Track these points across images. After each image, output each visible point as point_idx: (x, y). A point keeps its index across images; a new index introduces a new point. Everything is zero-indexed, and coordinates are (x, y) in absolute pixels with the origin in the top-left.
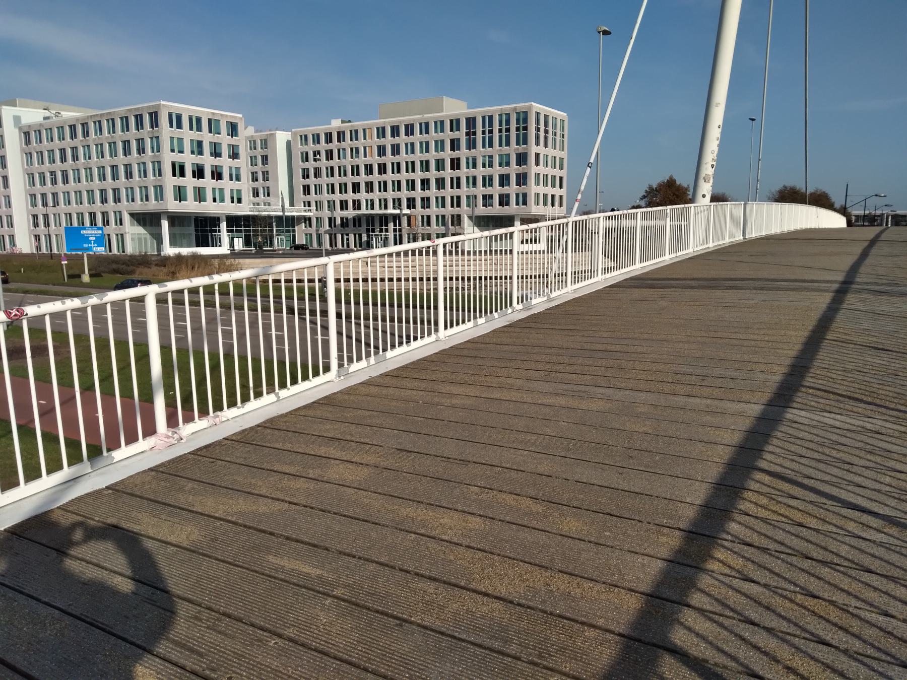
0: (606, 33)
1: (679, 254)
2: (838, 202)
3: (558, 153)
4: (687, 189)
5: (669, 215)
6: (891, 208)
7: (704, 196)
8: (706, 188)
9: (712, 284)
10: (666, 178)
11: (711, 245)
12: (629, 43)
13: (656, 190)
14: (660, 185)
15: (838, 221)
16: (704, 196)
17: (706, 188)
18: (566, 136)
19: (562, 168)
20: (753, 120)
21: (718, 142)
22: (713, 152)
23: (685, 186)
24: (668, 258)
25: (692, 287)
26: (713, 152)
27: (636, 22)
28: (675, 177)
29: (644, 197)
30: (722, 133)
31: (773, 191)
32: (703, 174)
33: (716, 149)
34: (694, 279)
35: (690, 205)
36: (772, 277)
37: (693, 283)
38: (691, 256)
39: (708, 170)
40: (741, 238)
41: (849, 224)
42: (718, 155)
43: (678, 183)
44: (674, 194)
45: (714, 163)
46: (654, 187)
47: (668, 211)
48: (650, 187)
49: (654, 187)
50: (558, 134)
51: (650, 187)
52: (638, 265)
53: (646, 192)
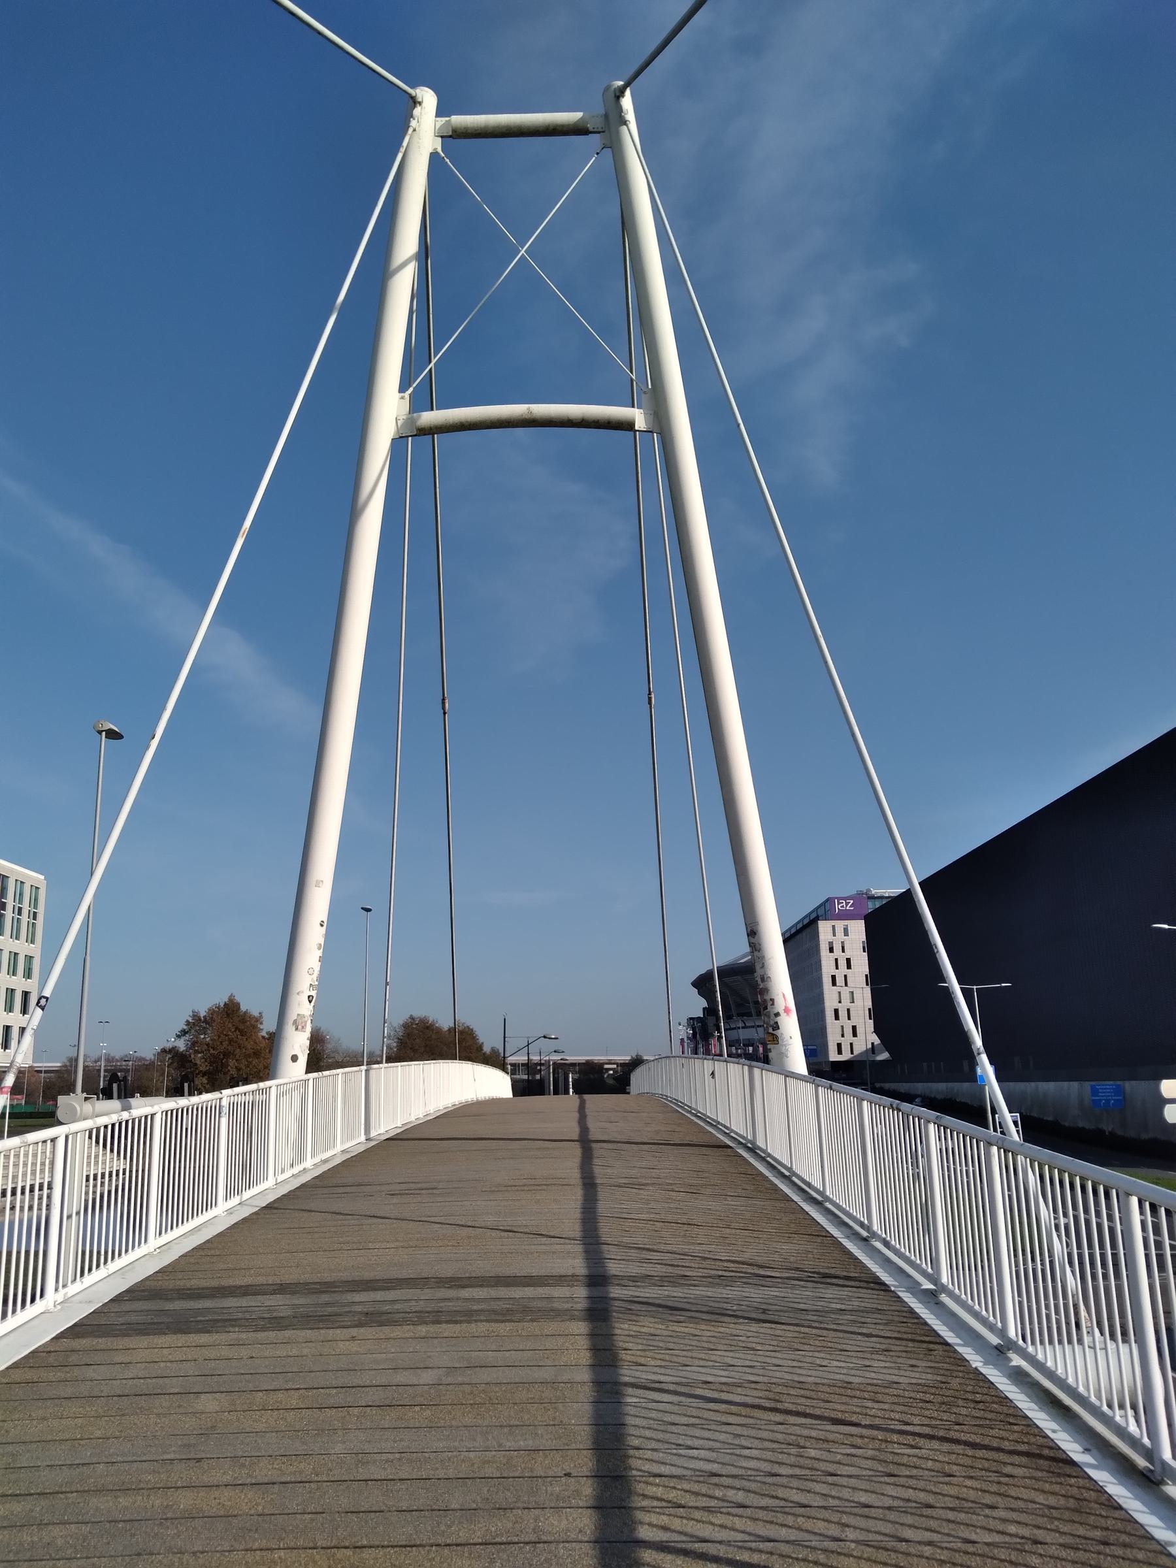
0: (112, 735)
1: (247, 1195)
2: (489, 1040)
3: (22, 947)
4: (258, 1020)
5: (225, 1110)
6: (553, 1045)
7: (294, 1058)
8: (297, 1043)
9: (324, 1304)
10: (221, 999)
11: (309, 1163)
12: (148, 747)
13: (205, 1021)
14: (212, 1012)
15: (495, 1084)
16: (294, 1058)
17: (297, 1043)
18: (40, 917)
19: (28, 974)
20: (368, 910)
21: (320, 953)
22: (310, 972)
23: (256, 1014)
24: (223, 1211)
25: (277, 1323)
26: (310, 972)
27: (164, 708)
28: (238, 999)
29: (184, 1033)
30: (327, 936)
31: (395, 1025)
32: (292, 1015)
33: (317, 966)
34: (282, 1289)
35: (268, 1083)
36: (448, 1271)
37: (280, 1304)
38: (271, 1198)
39: (301, 1007)
40: (363, 1138)
41: (520, 1089)
42: (321, 978)
43: (243, 1008)
44: (237, 1028)
45: (314, 993)
46: (202, 1014)
47: (225, 1102)
48: (195, 1016)
49: (202, 1014)
50: (25, 912)
51: (195, 1016)
52: (154, 1242)
53: (188, 1023)
